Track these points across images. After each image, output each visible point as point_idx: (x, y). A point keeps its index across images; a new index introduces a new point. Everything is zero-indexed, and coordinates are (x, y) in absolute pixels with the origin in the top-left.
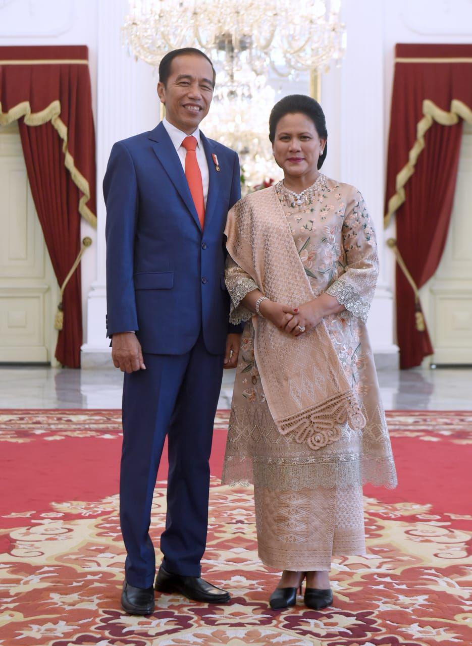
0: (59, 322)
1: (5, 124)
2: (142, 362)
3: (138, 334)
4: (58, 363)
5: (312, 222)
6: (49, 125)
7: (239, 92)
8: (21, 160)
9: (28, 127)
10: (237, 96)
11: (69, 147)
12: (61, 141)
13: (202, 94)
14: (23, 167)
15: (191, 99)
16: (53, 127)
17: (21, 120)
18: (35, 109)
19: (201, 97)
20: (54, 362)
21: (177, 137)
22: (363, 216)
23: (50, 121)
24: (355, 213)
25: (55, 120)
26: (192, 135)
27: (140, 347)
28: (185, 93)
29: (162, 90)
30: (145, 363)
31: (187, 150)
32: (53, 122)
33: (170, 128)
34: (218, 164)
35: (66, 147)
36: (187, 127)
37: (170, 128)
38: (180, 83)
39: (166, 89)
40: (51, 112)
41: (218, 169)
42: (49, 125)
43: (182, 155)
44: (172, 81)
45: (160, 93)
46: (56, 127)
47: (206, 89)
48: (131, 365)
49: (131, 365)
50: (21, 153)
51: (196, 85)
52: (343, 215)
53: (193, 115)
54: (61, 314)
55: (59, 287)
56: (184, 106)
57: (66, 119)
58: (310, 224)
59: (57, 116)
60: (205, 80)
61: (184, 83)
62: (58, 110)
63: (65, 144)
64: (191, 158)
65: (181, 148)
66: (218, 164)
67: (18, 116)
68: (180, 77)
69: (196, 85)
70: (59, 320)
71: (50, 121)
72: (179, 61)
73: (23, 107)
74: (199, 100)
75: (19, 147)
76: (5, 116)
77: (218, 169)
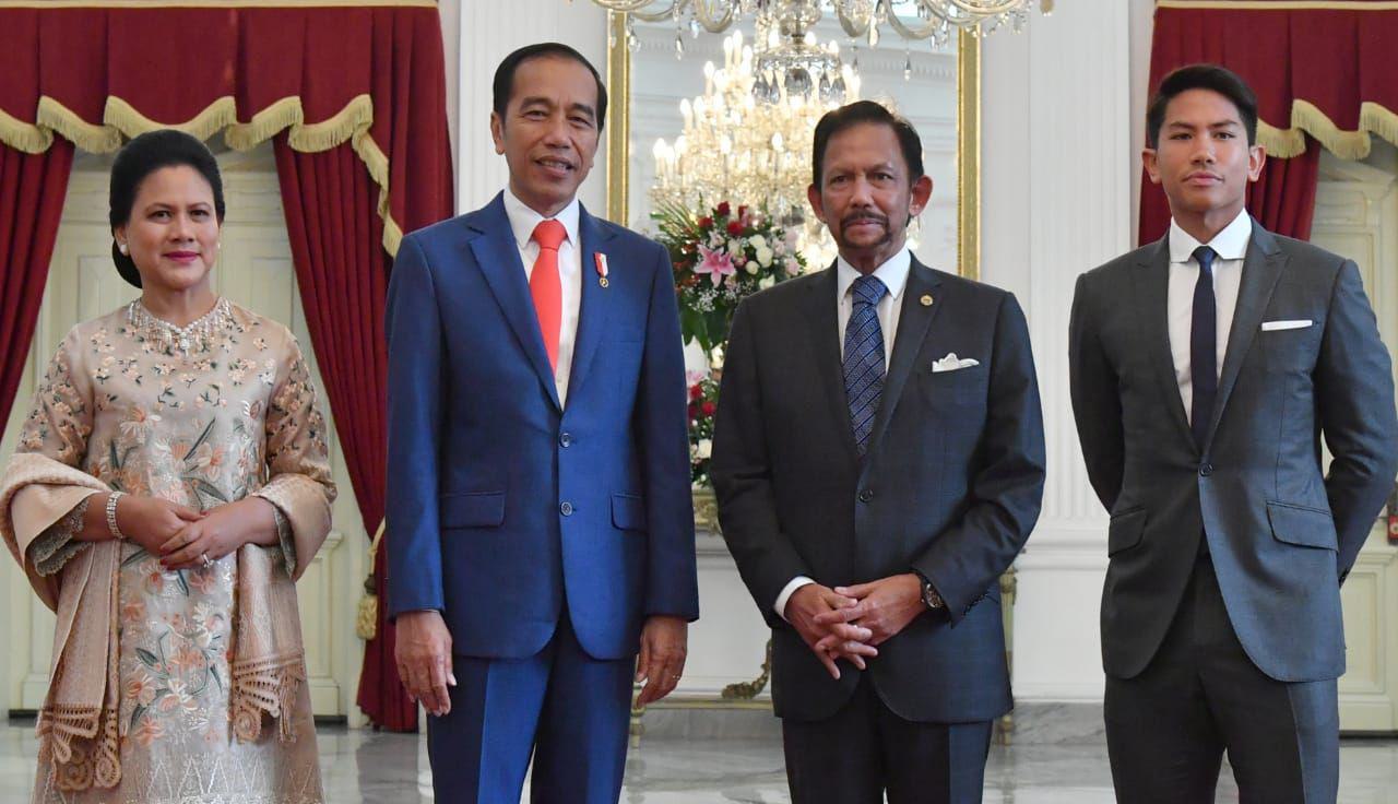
0: (366, 620)
1: (243, 148)
2: (450, 670)
3: (446, 616)
4: (366, 719)
5: (216, 388)
6: (346, 150)
7: (814, 73)
8: (282, 232)
9: (297, 154)
10: (810, 82)
11: (392, 203)
12: (374, 187)
13: (575, 138)
14: (285, 249)
15: (552, 146)
16: (355, 155)
17: (281, 139)
18: (311, 117)
19: (570, 143)
20: (356, 717)
21: (524, 220)
22: (306, 388)
23: (349, 141)
24: (292, 383)
25: (361, 138)
26: (556, 217)
27: (449, 640)
28: (537, 135)
29: (498, 127)
30: (455, 673)
31: (542, 247)
32: (355, 144)
33: (513, 204)
34: (605, 271)
35: (386, 203)
36: (544, 202)
37: (513, 204)
38: (529, 114)
39: (504, 128)
40: (351, 119)
41: (604, 283)
42: (346, 150)
43: (528, 259)
44: (513, 108)
45: (496, 133)
46: (362, 156)
47: (583, 125)
48: (430, 677)
49: (430, 677)
50: (282, 218)
51: (561, 116)
52: (272, 382)
53: (556, 179)
54: (372, 601)
55: (367, 538)
56: (539, 162)
57: (387, 139)
58: (212, 392)
59: (364, 129)
60: (578, 107)
61: (537, 113)
62: (368, 117)
63: (383, 198)
64: (546, 264)
65: (533, 244)
66: (605, 271)
67: (274, 131)
68: (529, 102)
69: (561, 116)
70: (368, 616)
71: (349, 141)
72: (526, 69)
73: (284, 110)
74: (567, 147)
75: (276, 202)
76: (246, 128)
77: (604, 283)
